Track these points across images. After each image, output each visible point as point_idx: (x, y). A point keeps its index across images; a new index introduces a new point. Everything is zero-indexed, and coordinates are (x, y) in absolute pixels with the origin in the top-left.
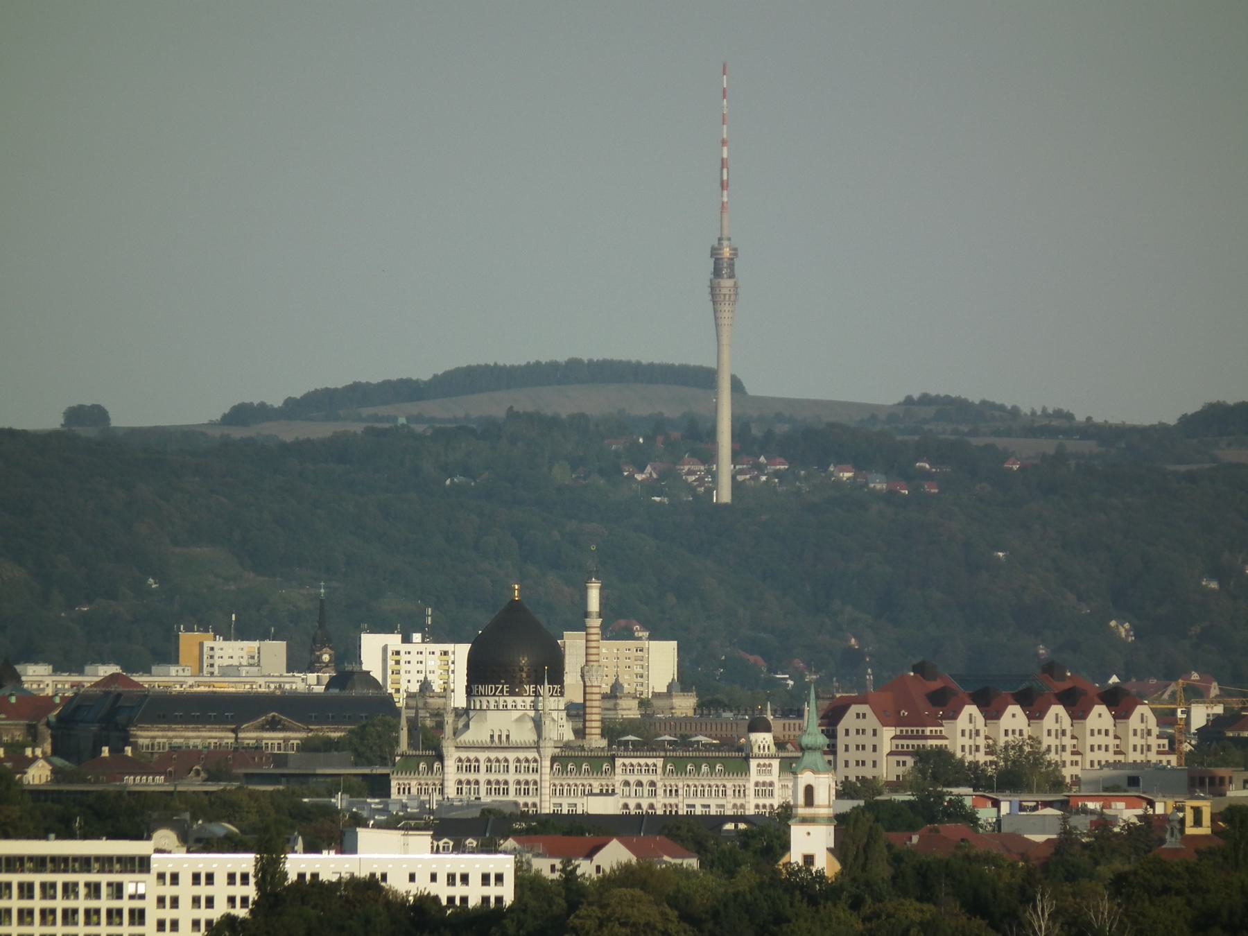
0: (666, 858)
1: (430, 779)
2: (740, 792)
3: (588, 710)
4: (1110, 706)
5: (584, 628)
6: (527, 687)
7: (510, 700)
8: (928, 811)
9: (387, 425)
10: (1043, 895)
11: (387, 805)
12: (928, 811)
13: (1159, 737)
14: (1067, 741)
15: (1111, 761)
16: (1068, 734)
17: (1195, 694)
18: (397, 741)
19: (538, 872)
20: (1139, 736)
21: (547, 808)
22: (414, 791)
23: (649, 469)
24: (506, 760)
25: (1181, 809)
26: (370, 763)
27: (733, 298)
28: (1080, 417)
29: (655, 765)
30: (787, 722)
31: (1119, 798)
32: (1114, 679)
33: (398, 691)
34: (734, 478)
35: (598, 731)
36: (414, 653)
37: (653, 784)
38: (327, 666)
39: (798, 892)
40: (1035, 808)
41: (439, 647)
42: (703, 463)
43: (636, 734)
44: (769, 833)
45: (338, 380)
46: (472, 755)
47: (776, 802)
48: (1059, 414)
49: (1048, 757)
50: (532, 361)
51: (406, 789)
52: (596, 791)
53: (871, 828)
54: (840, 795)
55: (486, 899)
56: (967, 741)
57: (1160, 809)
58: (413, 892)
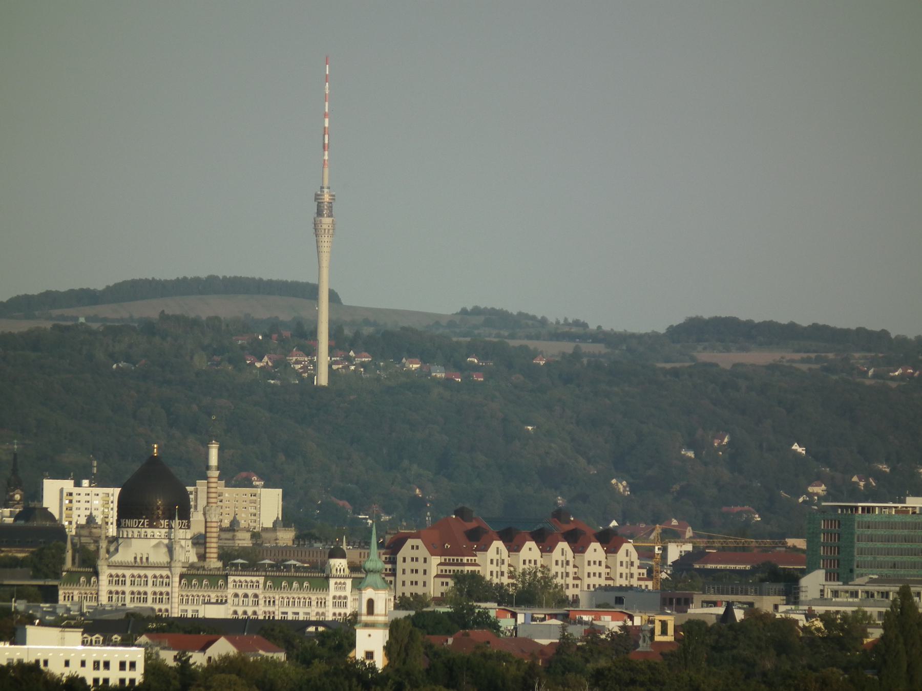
0: (261, 652)
1: (89, 590)
2: (322, 603)
3: (208, 540)
4: (603, 543)
5: (206, 478)
6: (162, 522)
7: (149, 531)
8: (462, 620)
9: (69, 323)
10: (539, 685)
11: (55, 608)
12: (462, 620)
13: (639, 567)
14: (570, 569)
15: (603, 585)
16: (571, 564)
17: (675, 536)
18: (63, 561)
19: (164, 660)
20: (626, 565)
21: (176, 613)
22: (76, 598)
23: (266, 359)
24: (146, 576)
25: (653, 622)
26: (46, 577)
27: (331, 231)
28: (593, 326)
29: (258, 582)
30: (363, 551)
31: (607, 613)
32: (614, 523)
33: (70, 523)
34: (330, 367)
35: (216, 555)
36: (83, 494)
37: (256, 596)
38: (18, 503)
39: (354, 680)
40: (543, 619)
41: (101, 491)
42: (307, 356)
43: (243, 557)
44: (341, 635)
45: (35, 289)
46: (120, 572)
47: (348, 611)
48: (577, 323)
49: (555, 581)
50: (181, 277)
51: (71, 597)
52: (213, 600)
53: (411, 632)
54: (397, 607)
55: (122, 681)
56: (494, 568)
57: (637, 621)
58: (67, 674)
